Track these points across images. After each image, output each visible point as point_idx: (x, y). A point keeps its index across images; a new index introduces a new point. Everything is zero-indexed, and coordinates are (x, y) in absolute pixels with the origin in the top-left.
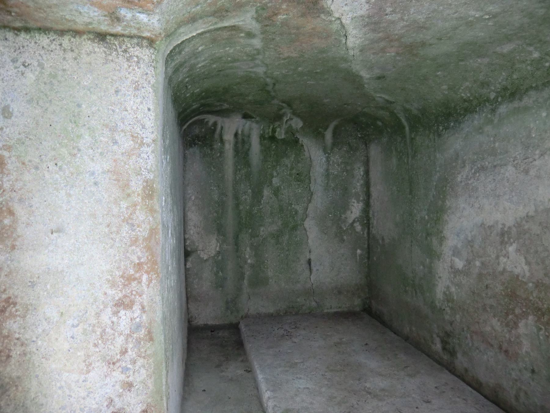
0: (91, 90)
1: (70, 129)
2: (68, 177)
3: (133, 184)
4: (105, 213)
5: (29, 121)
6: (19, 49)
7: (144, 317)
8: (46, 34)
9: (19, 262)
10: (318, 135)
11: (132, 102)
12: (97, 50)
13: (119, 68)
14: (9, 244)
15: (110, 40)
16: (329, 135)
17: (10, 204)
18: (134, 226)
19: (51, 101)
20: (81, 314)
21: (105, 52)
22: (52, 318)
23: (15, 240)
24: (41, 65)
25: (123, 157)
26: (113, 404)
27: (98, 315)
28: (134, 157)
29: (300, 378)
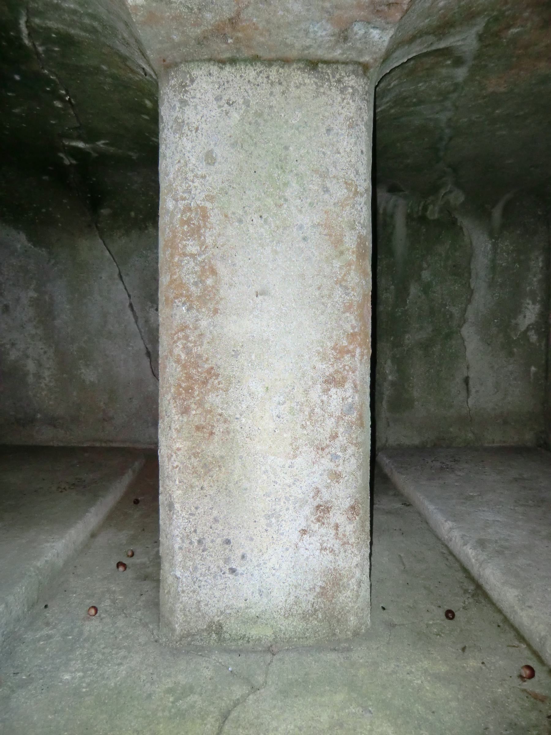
0: (300, 129)
1: (276, 175)
2: (274, 231)
3: (346, 239)
4: (316, 273)
5: (232, 167)
6: (224, 84)
7: (357, 398)
8: (252, 65)
9: (222, 328)
10: (482, 213)
11: (345, 143)
12: (307, 81)
13: (331, 101)
14: (211, 306)
15: (322, 68)
16: (497, 213)
17: (213, 262)
18: (348, 289)
19: (256, 143)
20: (287, 390)
21: (316, 83)
22: (256, 394)
23: (217, 303)
24: (247, 103)
25: (335, 207)
26: (319, 495)
27: (306, 392)
28: (348, 208)
29: (484, 511)
